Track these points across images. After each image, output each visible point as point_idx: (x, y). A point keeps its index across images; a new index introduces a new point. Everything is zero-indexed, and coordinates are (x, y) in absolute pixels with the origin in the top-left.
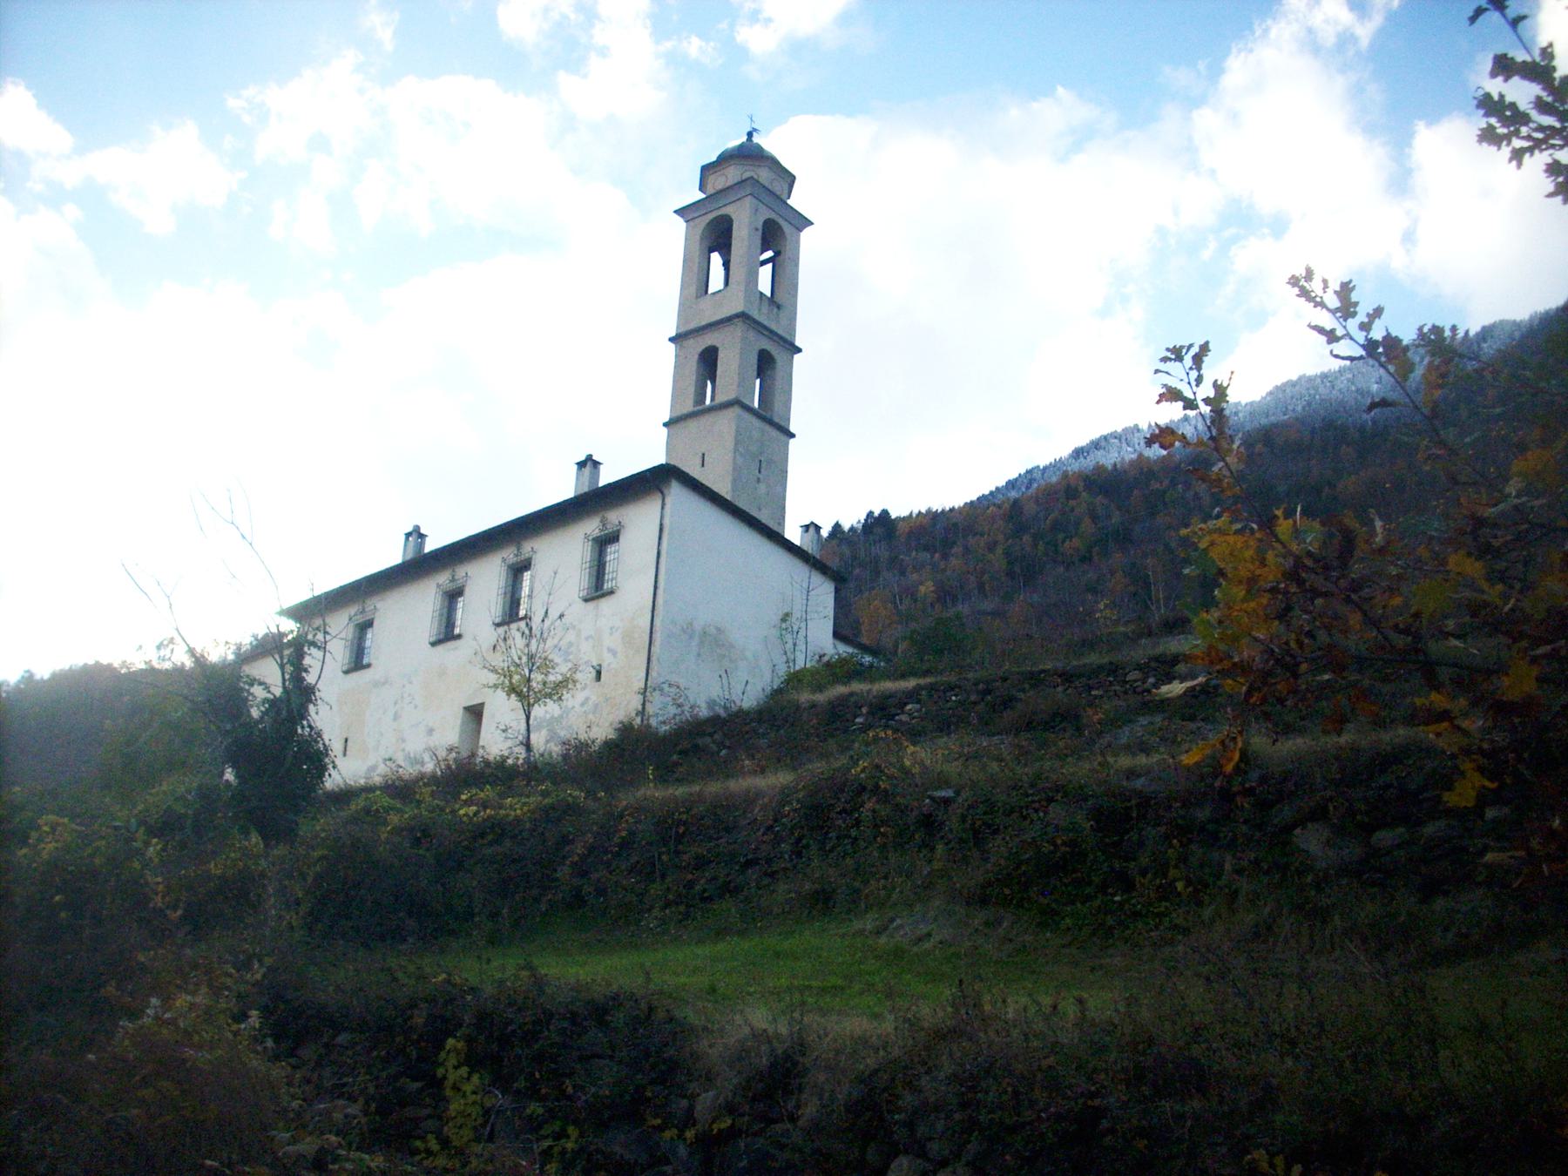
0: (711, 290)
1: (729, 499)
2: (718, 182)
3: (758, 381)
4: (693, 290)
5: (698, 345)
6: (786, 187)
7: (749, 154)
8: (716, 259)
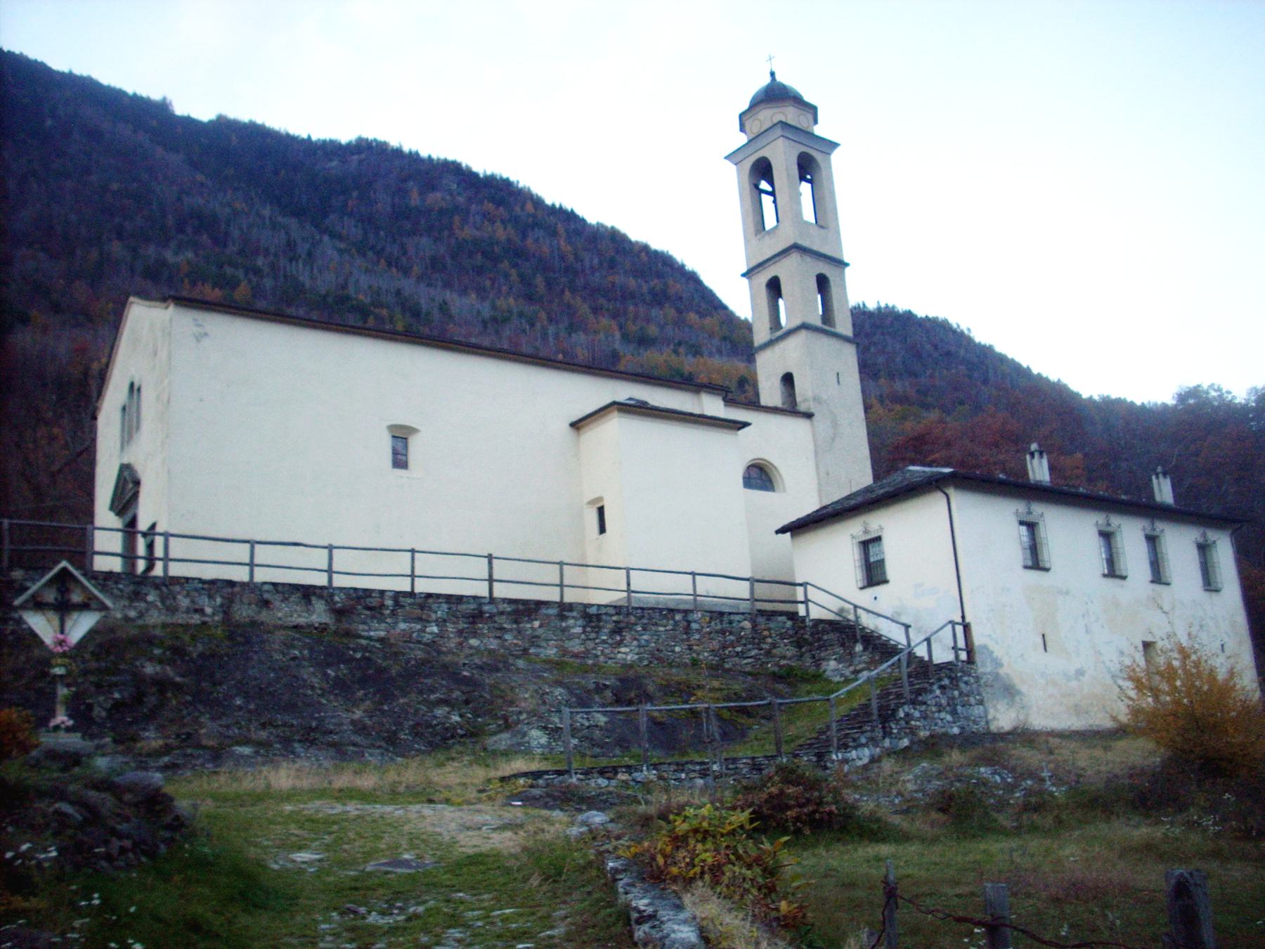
0: (767, 228)
1: (798, 400)
2: (755, 126)
3: (819, 297)
4: (752, 229)
5: (764, 278)
6: (810, 117)
7: (775, 94)
8: (767, 200)
